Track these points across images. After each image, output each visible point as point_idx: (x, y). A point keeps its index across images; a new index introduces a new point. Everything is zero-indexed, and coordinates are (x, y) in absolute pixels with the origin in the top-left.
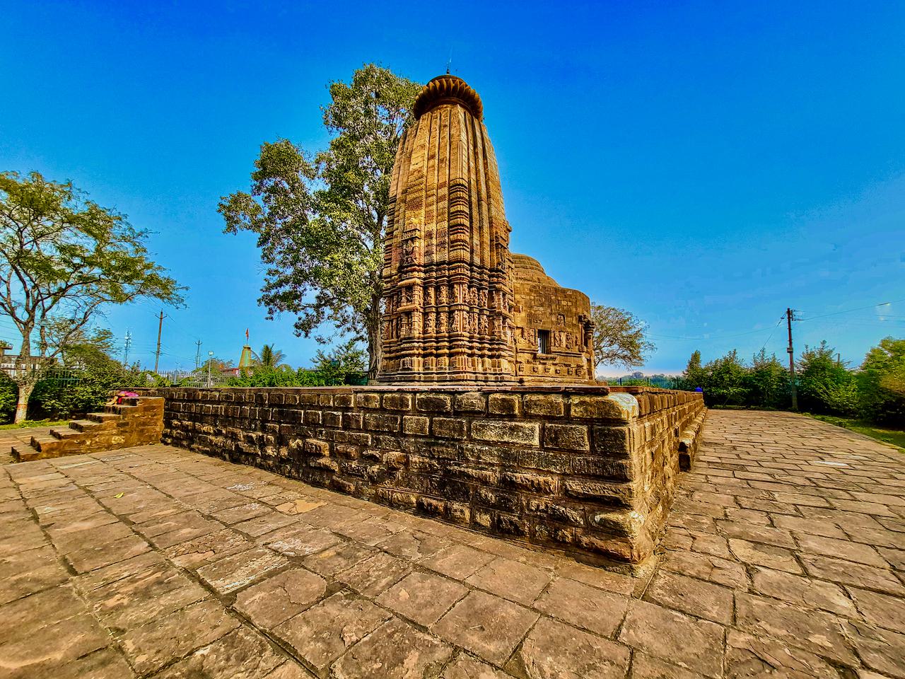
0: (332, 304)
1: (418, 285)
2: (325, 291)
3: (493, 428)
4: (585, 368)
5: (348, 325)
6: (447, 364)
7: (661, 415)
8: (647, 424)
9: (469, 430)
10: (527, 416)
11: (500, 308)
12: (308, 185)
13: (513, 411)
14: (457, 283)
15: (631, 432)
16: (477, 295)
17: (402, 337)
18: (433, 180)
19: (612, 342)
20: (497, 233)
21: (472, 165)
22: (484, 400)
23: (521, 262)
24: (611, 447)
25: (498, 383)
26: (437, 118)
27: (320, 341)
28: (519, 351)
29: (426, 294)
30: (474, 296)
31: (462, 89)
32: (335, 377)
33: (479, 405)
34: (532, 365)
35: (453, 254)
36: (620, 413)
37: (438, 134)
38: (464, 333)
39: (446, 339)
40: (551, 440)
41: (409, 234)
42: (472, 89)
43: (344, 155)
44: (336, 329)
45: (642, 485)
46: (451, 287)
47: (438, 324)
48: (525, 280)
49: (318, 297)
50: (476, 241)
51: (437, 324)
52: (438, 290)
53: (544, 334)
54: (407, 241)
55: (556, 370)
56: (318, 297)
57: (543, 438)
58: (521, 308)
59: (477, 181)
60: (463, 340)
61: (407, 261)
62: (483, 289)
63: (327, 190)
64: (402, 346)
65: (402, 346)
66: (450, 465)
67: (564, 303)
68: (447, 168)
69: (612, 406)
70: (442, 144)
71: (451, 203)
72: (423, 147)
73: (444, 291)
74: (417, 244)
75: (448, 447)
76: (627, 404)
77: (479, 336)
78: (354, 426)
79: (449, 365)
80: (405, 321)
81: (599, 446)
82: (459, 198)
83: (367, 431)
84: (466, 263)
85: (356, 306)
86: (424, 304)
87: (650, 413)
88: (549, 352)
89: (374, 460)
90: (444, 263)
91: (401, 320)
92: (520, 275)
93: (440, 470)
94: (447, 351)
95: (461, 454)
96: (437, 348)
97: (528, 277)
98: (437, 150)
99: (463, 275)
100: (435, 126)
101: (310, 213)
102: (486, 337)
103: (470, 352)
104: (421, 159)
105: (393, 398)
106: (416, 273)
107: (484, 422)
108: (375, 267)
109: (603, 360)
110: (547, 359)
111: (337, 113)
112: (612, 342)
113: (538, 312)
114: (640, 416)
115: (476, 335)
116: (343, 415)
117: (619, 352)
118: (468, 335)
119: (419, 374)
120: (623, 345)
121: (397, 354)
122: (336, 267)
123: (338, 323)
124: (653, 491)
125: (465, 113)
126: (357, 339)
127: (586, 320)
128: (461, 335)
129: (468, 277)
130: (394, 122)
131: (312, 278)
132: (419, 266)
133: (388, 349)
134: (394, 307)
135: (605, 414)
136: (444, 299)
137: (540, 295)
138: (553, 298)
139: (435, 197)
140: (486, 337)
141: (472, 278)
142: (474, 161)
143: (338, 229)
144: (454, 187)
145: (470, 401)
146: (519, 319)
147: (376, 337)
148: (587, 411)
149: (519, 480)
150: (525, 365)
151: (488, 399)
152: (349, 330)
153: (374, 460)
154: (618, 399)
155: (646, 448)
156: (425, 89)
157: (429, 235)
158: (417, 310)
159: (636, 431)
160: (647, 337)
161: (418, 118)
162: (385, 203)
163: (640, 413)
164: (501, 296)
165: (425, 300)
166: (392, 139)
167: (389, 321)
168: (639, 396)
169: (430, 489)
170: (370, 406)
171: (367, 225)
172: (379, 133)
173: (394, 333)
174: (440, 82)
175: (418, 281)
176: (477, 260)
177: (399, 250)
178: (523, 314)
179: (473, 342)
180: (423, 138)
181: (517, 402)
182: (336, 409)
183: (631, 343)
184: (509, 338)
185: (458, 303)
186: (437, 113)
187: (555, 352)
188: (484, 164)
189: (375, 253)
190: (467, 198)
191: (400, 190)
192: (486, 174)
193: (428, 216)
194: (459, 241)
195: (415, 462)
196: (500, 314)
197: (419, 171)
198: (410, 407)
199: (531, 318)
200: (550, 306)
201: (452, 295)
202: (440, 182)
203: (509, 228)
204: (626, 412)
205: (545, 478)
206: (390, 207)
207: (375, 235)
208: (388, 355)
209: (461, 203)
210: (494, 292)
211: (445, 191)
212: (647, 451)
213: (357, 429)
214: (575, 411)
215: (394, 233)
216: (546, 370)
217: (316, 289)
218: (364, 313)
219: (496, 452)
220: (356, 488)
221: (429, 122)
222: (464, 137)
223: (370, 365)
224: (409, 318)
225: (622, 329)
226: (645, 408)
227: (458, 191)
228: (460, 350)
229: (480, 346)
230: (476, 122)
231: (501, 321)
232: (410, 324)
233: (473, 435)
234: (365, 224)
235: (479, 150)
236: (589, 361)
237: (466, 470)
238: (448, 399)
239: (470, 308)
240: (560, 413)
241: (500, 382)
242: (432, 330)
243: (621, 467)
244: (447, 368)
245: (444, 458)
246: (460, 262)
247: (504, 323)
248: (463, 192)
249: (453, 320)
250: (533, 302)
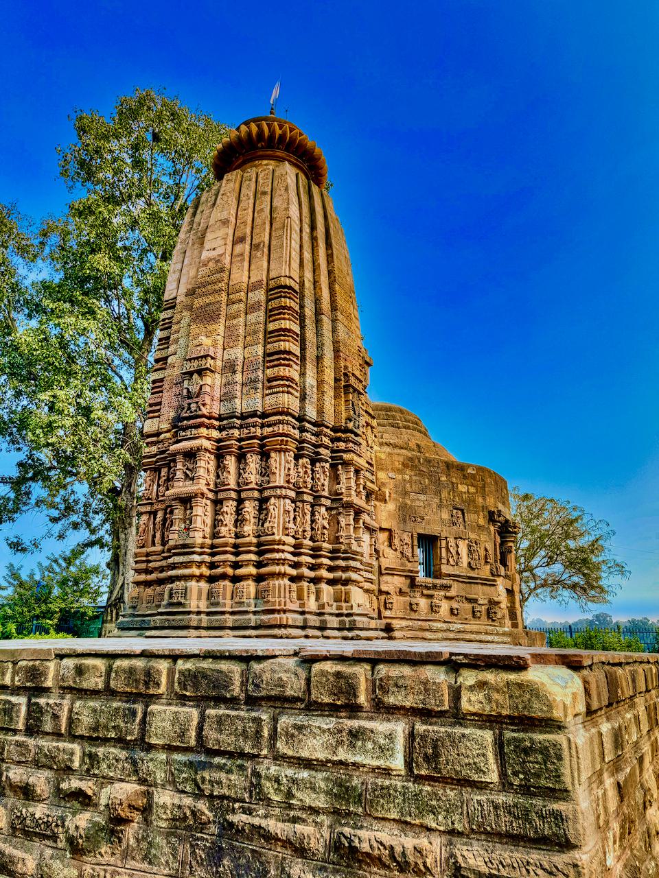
0: (47, 478)
1: (206, 450)
2: (37, 454)
3: (318, 731)
4: (503, 605)
5: (74, 518)
6: (252, 595)
7: (633, 706)
8: (605, 727)
9: (274, 736)
10: (382, 709)
11: (349, 495)
12: (22, 271)
13: (356, 696)
14: (276, 450)
15: (573, 746)
16: (309, 472)
17: (171, 543)
18: (240, 276)
19: (551, 558)
20: (346, 367)
21: (307, 256)
22: (303, 674)
23: (388, 417)
24: (537, 775)
25: (346, 633)
26: (250, 180)
27: (17, 546)
28: (384, 572)
29: (220, 467)
30: (306, 472)
31: (293, 140)
32: (37, 617)
33: (294, 687)
34: (408, 598)
35: (270, 400)
36: (550, 707)
37: (251, 205)
38: (285, 538)
39: (252, 548)
40: (427, 758)
41: (196, 363)
42: (310, 140)
43: (92, 226)
44: (51, 524)
45: (601, 855)
46: (265, 456)
47: (239, 521)
48: (395, 446)
49: (20, 465)
50: (311, 380)
51: (236, 521)
52: (241, 458)
53: (428, 542)
54: (190, 374)
55: (452, 609)
56: (20, 464)
57: (411, 753)
58: (387, 495)
59: (315, 283)
60: (283, 551)
61: (189, 408)
62: (321, 460)
63: (57, 281)
64: (170, 561)
65: (170, 561)
66: (233, 811)
67: (463, 488)
68: (265, 258)
69: (533, 691)
70: (258, 221)
71: (271, 316)
72: (225, 222)
73: (253, 462)
74: (208, 380)
75: (230, 772)
76: (560, 688)
77: (311, 543)
78: (48, 726)
79: (256, 598)
80: (178, 513)
81: (515, 774)
82: (284, 308)
83: (74, 737)
84: (293, 417)
85: (94, 483)
86: (216, 484)
87: (610, 705)
88: (438, 575)
89: (83, 799)
90: (254, 414)
91: (172, 512)
92: (387, 438)
93: (214, 822)
94: (253, 571)
95: (255, 788)
96: (236, 565)
97: (400, 442)
98: (248, 230)
99: (287, 435)
100: (248, 192)
101: (21, 316)
102: (325, 545)
103: (294, 572)
104: (222, 242)
105: (131, 671)
106: (203, 431)
107: (300, 719)
108: (131, 415)
109: (539, 591)
110: (434, 587)
111: (85, 160)
112: (551, 558)
113: (417, 503)
114: (590, 712)
115: (307, 542)
116: (29, 704)
117: (565, 576)
118: (293, 541)
119: (199, 613)
120: (570, 564)
121: (158, 576)
122: (60, 412)
123: (56, 513)
124: (625, 866)
125: (297, 175)
126: (91, 544)
127: (501, 519)
128: (280, 542)
129: (296, 440)
130: (182, 180)
131: (15, 429)
132: (210, 418)
133: (143, 566)
134: (161, 489)
135: (525, 707)
136: (253, 477)
137: (421, 473)
138: (444, 478)
139: (242, 305)
140: (325, 545)
141: (302, 441)
142: (310, 250)
143: (72, 346)
144: (276, 290)
145: (276, 676)
146: (385, 514)
147: (126, 540)
148: (490, 700)
149: (365, 847)
150: (395, 599)
151: (310, 673)
152: (76, 526)
153: (83, 799)
154: (545, 679)
155: (606, 775)
156: (233, 135)
157: (230, 367)
158: (203, 494)
159: (580, 742)
160: (613, 551)
161: (219, 177)
162: (159, 307)
163: (588, 706)
164: (352, 474)
165: (218, 477)
166: (177, 207)
167: (150, 513)
168: (585, 672)
169: (191, 867)
170: (85, 685)
171: (125, 343)
172: (156, 195)
173: (158, 535)
174: (258, 126)
175: (207, 444)
176: (311, 413)
177: (176, 390)
178: (391, 506)
179: (300, 554)
180: (226, 209)
181: (362, 679)
182: (16, 691)
183: (585, 561)
184: (365, 548)
185: (277, 484)
186: (251, 172)
187: (449, 575)
188: (327, 255)
189: (136, 390)
190: (297, 308)
191: (183, 290)
192: (330, 272)
193: (230, 334)
194: (282, 378)
195: (164, 807)
196: (349, 505)
197: (217, 261)
198: (163, 689)
199: (406, 514)
200: (438, 493)
201: (266, 471)
202: (252, 280)
203: (368, 360)
204: (561, 706)
205: (416, 841)
206: (163, 315)
207: (137, 361)
208: (143, 577)
209: (286, 316)
210: (340, 467)
211: (260, 295)
212: (609, 782)
213: (53, 734)
214: (469, 700)
215: (169, 360)
216: (433, 609)
217: (19, 449)
218: (107, 496)
219: (322, 784)
220: (39, 866)
221: (237, 185)
222: (294, 211)
223: (111, 592)
224: (186, 509)
225: (567, 536)
226: (599, 695)
227: (281, 297)
228: (276, 569)
229: (313, 561)
230: (315, 189)
231: (352, 517)
232: (189, 520)
233: (281, 746)
234: (121, 341)
235: (318, 234)
236: (510, 592)
237: (263, 823)
238: (234, 670)
239: (298, 493)
240: (442, 702)
241: (350, 629)
242: (227, 530)
243: (558, 817)
244: (252, 602)
245: (223, 797)
246: (281, 413)
247: (356, 520)
248: (290, 298)
249: (267, 515)
250: (408, 485)
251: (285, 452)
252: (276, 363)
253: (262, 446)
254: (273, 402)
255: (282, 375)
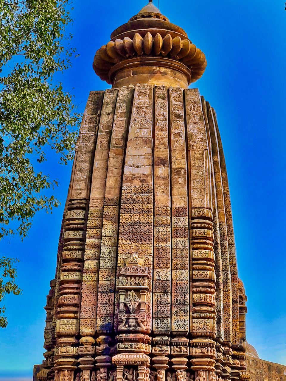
61: (127, 322)
71: (193, 244)
144: (197, 220)
251: (209, 371)
252: (202, 289)
253: (189, 364)
254: (201, 325)
255: (209, 302)
